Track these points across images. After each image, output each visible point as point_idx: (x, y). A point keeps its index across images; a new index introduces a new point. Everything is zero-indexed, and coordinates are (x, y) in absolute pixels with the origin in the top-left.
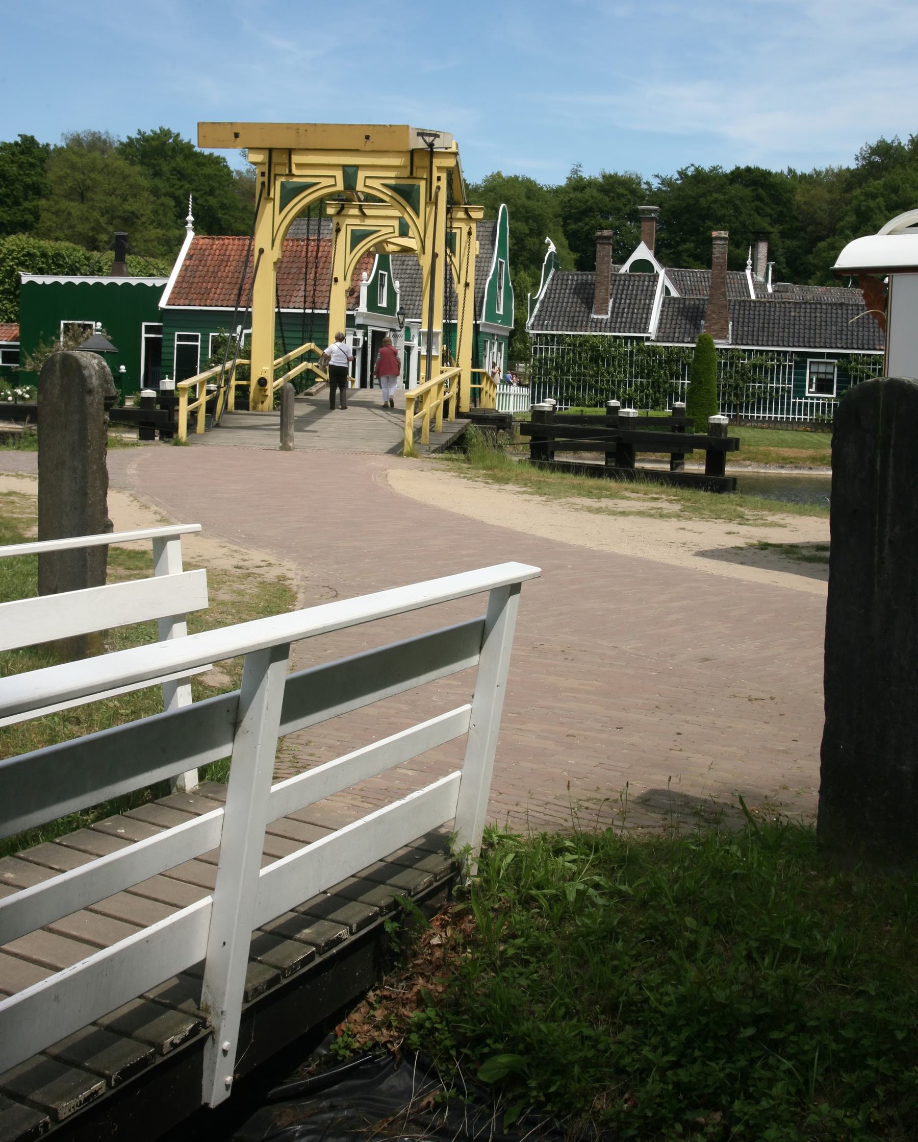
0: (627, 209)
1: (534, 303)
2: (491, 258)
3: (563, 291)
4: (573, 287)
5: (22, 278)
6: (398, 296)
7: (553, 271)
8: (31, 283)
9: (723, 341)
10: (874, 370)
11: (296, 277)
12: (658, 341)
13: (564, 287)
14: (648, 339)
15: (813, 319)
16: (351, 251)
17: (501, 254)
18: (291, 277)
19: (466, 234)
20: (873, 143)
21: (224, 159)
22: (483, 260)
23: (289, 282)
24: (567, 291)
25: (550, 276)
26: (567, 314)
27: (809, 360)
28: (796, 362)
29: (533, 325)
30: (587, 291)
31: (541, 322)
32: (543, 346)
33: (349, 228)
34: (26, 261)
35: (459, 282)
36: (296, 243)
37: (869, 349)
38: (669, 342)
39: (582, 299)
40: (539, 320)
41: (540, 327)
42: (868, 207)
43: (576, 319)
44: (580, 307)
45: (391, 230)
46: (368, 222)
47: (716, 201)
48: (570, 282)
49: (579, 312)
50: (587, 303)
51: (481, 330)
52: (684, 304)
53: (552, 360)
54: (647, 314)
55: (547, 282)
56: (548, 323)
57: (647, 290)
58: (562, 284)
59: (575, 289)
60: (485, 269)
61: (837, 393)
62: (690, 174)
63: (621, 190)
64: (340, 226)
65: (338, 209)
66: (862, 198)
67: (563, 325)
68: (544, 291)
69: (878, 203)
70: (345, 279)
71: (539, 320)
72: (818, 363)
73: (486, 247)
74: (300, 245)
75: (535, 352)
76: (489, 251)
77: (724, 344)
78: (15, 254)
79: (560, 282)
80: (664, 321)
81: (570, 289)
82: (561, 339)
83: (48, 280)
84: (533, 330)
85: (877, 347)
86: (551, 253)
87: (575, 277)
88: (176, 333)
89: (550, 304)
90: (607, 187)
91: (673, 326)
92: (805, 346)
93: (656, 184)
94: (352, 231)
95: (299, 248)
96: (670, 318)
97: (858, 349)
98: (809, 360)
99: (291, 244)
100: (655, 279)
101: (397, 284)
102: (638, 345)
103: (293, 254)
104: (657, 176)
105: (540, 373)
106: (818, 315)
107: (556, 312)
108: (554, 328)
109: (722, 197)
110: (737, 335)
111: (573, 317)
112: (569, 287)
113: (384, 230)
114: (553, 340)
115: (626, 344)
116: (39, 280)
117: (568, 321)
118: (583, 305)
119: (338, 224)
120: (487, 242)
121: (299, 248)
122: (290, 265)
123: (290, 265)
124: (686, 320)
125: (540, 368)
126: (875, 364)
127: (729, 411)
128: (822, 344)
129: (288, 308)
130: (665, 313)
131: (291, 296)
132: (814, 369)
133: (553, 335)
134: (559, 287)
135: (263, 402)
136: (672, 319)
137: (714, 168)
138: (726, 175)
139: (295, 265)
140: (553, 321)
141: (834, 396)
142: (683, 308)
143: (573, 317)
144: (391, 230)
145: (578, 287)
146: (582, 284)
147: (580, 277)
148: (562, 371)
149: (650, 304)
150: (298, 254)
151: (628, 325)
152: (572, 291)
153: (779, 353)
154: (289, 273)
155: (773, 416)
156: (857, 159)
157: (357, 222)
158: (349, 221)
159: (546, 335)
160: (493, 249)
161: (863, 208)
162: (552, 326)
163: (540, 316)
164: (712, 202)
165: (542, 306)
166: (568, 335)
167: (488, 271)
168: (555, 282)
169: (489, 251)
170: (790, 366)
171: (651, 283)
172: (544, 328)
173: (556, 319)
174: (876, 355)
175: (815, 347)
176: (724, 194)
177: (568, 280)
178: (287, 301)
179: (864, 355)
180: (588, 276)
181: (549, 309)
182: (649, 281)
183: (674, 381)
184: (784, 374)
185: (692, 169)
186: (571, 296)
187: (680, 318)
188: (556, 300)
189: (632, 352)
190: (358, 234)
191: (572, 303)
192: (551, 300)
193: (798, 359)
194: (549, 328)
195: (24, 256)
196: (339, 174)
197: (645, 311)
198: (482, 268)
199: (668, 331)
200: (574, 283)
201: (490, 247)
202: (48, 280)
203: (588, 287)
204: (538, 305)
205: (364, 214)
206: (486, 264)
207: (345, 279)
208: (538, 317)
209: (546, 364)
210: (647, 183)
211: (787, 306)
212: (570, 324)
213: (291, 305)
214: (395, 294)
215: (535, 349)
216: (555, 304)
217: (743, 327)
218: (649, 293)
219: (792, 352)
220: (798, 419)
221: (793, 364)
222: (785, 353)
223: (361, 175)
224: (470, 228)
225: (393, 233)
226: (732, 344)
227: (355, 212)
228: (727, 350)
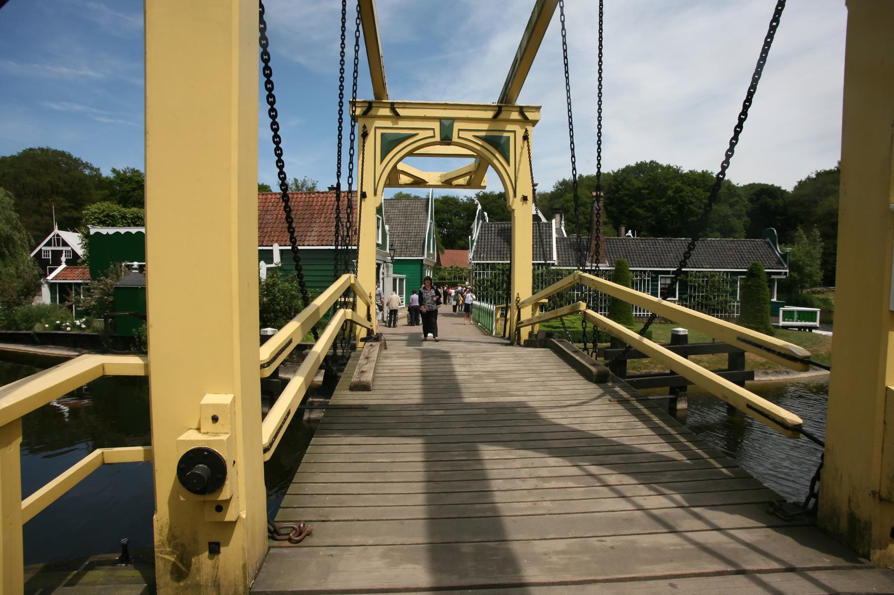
0: (454, 211)
1: (473, 242)
2: (427, 219)
3: (490, 235)
4: (496, 232)
5: (90, 230)
6: (388, 236)
7: (481, 222)
8: (97, 233)
9: (603, 265)
10: (703, 281)
11: (309, 221)
12: (560, 266)
13: (490, 232)
14: (553, 265)
15: (656, 249)
16: (382, 160)
17: (431, 219)
18: (305, 221)
19: (521, 138)
20: (561, 180)
21: (269, 186)
22: (422, 221)
23: (303, 225)
24: (493, 235)
25: (480, 225)
26: (495, 249)
27: (660, 276)
28: (652, 277)
29: (473, 257)
30: (506, 234)
31: (479, 255)
32: (481, 272)
33: (379, 132)
34: (107, 221)
35: (515, 196)
36: (308, 196)
37: (699, 268)
38: (567, 266)
39: (503, 239)
40: (477, 254)
41: (478, 258)
42: (567, 206)
43: (502, 253)
44: (504, 245)
45: (430, 133)
46: (402, 124)
47: (494, 206)
48: (493, 229)
49: (504, 248)
50: (507, 242)
51: (424, 263)
52: (570, 241)
53: (487, 281)
54: (550, 248)
55: (479, 229)
56: (483, 256)
57: (546, 233)
58: (488, 230)
59: (498, 233)
60: (424, 226)
61: (679, 297)
62: (481, 195)
63: (451, 202)
64: (368, 129)
65: (365, 109)
66: (564, 202)
67: (494, 257)
68: (478, 234)
69: (572, 204)
70: (375, 194)
71: (477, 254)
72: (666, 277)
73: (423, 213)
74: (312, 197)
75: (476, 275)
76: (425, 216)
77: (604, 267)
78: (96, 215)
79: (486, 229)
80: (560, 253)
81: (495, 233)
82: (493, 267)
83: (111, 231)
84: (474, 260)
85: (704, 266)
86: (480, 210)
87: (497, 226)
88: (123, 264)
89: (483, 244)
90: (445, 201)
91: (567, 256)
92: (658, 267)
93: (465, 200)
94: (382, 135)
95: (311, 199)
96: (563, 250)
97: (692, 268)
98: (660, 276)
99: (304, 197)
100: (549, 225)
101: (387, 227)
102: (546, 268)
103: (306, 204)
104: (465, 197)
105: (480, 290)
106: (658, 246)
107: (487, 248)
108: (489, 259)
109: (496, 205)
110: (611, 260)
111: (500, 251)
112: (493, 232)
113: (422, 134)
114: (488, 267)
115: (538, 269)
116: (104, 231)
117: (497, 254)
118: (505, 243)
119: (365, 127)
120: (423, 211)
121: (311, 199)
122: (303, 212)
123: (303, 212)
124: (571, 249)
125: (479, 287)
126: (703, 277)
127: (601, 311)
128: (669, 266)
129: (304, 245)
130: (559, 248)
131: (305, 236)
132: (663, 282)
133: (488, 264)
134: (487, 232)
135: (214, 549)
136: (565, 251)
137: (491, 192)
138: (496, 195)
139: (308, 212)
140: (487, 254)
141: (677, 299)
142: (570, 244)
143: (500, 251)
144: (430, 133)
145: (500, 232)
146: (501, 229)
147: (500, 226)
148: (495, 288)
149: (550, 242)
150: (310, 204)
151: (538, 256)
152: (496, 234)
153: (641, 271)
154: (303, 218)
155: (638, 313)
156: (554, 187)
157: (388, 124)
158: (378, 123)
159: (483, 264)
160: (428, 214)
161: (565, 206)
162: (487, 258)
163: (477, 251)
164: (492, 207)
165: (477, 245)
166: (499, 264)
167: (426, 227)
168: (483, 229)
169: (425, 216)
170: (648, 280)
171: (548, 228)
172: (482, 259)
173: (489, 253)
174: (705, 271)
175: (665, 267)
176: (497, 203)
177: (492, 227)
178: (302, 240)
179: (697, 271)
180: (508, 225)
181: (483, 246)
182: (546, 227)
183: (572, 292)
184: (644, 285)
185: (482, 193)
186: (496, 237)
187: (570, 250)
188: (486, 240)
189: (542, 274)
190: (390, 139)
191: (498, 242)
192: (483, 241)
193: (654, 275)
194: (485, 259)
195: (104, 216)
196: (436, 125)
197: (548, 246)
198: (421, 226)
199: (564, 259)
200: (497, 229)
201: (425, 213)
202: (111, 231)
203: (506, 231)
204: (475, 244)
205: (397, 114)
206: (424, 223)
207: (375, 194)
208: (476, 252)
209: (484, 283)
210: (462, 199)
211: (637, 241)
212: (499, 256)
213: (306, 243)
214: (386, 234)
215: (476, 273)
216: (486, 243)
217: (613, 255)
218: (548, 235)
219: (650, 271)
220: (643, 314)
221: (650, 279)
222: (644, 272)
223: (457, 126)
224: (527, 130)
225: (434, 137)
226: (609, 267)
227: (386, 112)
228: (606, 270)
